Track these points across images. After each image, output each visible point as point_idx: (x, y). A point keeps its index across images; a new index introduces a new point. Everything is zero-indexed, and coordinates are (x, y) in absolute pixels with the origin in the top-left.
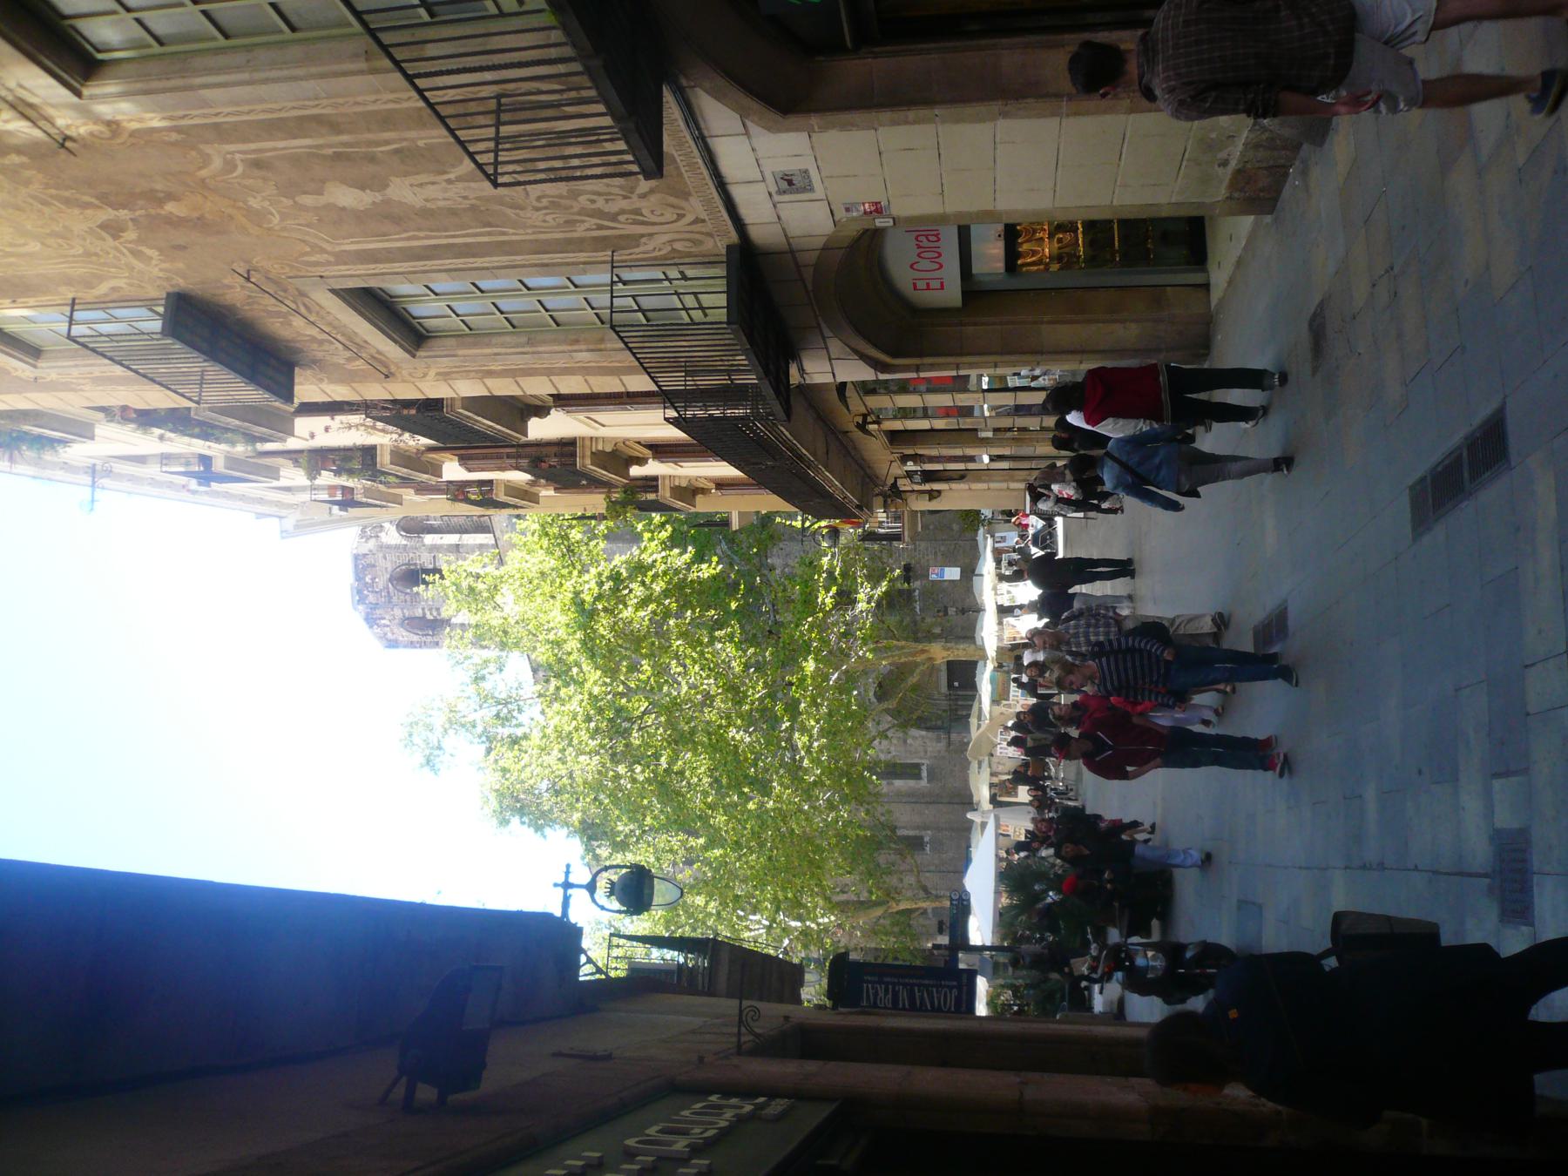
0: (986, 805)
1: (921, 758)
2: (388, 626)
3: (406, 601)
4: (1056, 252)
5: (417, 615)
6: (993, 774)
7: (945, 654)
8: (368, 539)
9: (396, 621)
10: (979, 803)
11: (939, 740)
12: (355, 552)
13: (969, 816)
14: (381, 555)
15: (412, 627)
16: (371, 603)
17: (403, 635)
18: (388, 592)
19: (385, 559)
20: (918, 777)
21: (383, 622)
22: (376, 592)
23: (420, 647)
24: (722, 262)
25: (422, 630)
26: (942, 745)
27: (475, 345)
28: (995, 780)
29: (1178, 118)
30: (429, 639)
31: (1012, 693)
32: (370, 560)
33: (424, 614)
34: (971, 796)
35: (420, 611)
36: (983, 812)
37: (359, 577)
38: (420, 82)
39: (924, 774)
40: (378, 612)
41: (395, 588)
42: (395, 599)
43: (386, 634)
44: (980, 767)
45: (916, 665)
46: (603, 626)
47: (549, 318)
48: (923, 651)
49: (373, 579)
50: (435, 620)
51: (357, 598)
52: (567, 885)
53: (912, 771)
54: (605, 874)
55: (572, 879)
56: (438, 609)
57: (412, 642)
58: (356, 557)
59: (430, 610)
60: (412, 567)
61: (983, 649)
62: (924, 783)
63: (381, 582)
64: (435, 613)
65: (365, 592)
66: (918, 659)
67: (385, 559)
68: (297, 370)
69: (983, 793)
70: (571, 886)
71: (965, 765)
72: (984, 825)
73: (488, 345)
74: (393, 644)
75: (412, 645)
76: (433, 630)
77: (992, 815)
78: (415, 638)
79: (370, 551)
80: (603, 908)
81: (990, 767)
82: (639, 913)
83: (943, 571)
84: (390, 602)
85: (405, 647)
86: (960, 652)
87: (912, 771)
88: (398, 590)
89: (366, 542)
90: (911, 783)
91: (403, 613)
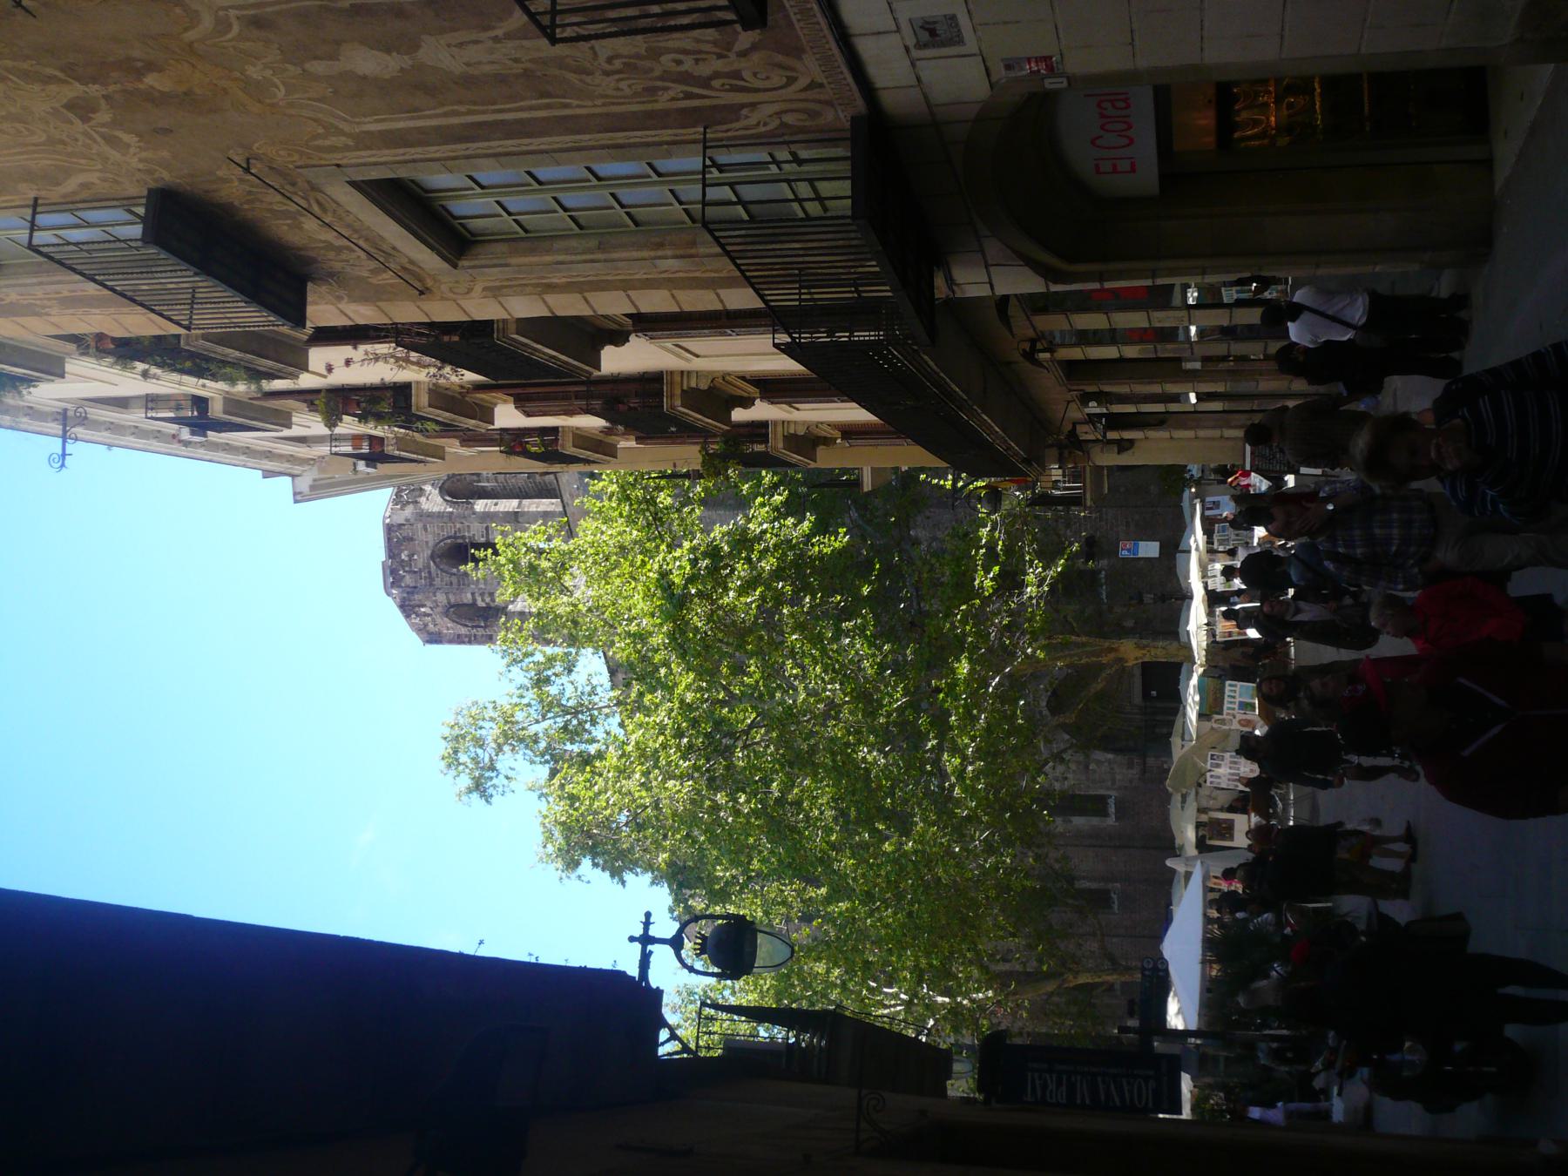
0: (1191, 850)
1: (1108, 789)
2: (429, 615)
5: (465, 601)
6: (1201, 810)
7: (1139, 653)
10: (1182, 847)
11: (1130, 766)
13: (1169, 863)
15: (460, 617)
17: (448, 626)
18: (430, 572)
20: (1105, 814)
21: (423, 610)
22: (415, 572)
23: (470, 642)
25: (471, 620)
26: (1134, 772)
27: (533, 251)
28: (1204, 818)
30: (481, 632)
31: (1226, 705)
33: (474, 600)
34: (1173, 839)
35: (469, 596)
36: (1188, 859)
39: (1112, 809)
41: (437, 566)
43: (426, 625)
44: (1184, 801)
45: (1102, 667)
46: (697, 617)
48: (1111, 650)
49: (411, 556)
50: (488, 608)
53: (1097, 805)
57: (459, 636)
59: (482, 595)
61: (1189, 647)
62: (1111, 821)
63: (421, 559)
66: (1104, 660)
68: (310, 286)
69: (1190, 834)
71: (1166, 798)
72: (1188, 875)
73: (548, 251)
74: (433, 638)
75: (459, 640)
76: (486, 619)
77: (1199, 863)
78: (463, 631)
81: (1196, 800)
83: (1136, 546)
85: (451, 642)
86: (1159, 651)
87: (1097, 805)
88: (441, 570)
90: (1095, 821)
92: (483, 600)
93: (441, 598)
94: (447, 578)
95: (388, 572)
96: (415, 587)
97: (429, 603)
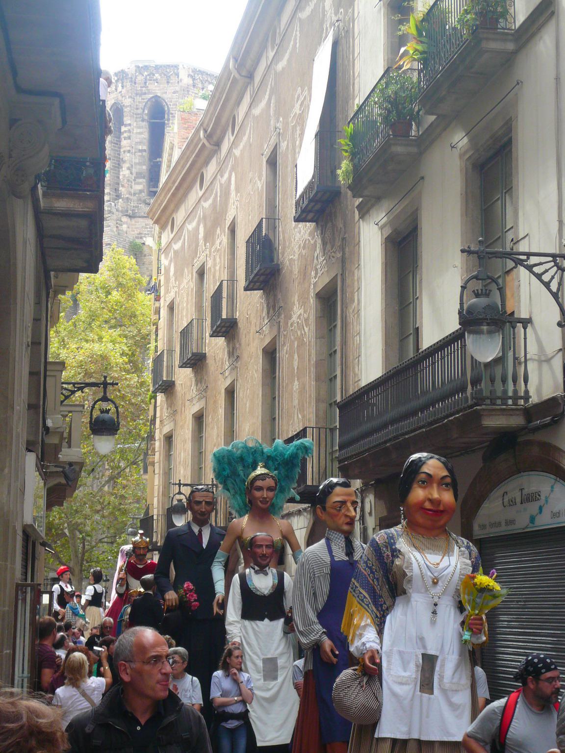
2: (116, 89)
3: (137, 109)
4: (129, 118)
5: (125, 119)
8: (192, 76)
9: (120, 98)
12: (181, 67)
14: (177, 89)
16: (136, 76)
18: (145, 94)
19: (174, 93)
21: (120, 85)
22: (145, 83)
24: (50, 370)
29: (465, 735)
32: (173, 79)
33: (126, 125)
35: (129, 122)
37: (157, 68)
38: (536, 269)
40: (129, 84)
42: (139, 99)
47: (498, 236)
49: (156, 81)
51: (141, 65)
52: (105, 384)
54: (113, 409)
55: (110, 388)
56: (129, 138)
58: (176, 67)
59: (129, 131)
60: (166, 116)
63: (156, 89)
64: (126, 135)
65: (146, 73)
67: (174, 93)
70: (105, 388)
79: (181, 80)
80: (93, 407)
82: (91, 428)
84: (137, 94)
88: (146, 103)
89: (189, 75)
91: (127, 107)
92: (125, 131)
93: (127, 102)
94: (141, 106)
95: (146, 64)
96: (135, 83)
97: (124, 91)
